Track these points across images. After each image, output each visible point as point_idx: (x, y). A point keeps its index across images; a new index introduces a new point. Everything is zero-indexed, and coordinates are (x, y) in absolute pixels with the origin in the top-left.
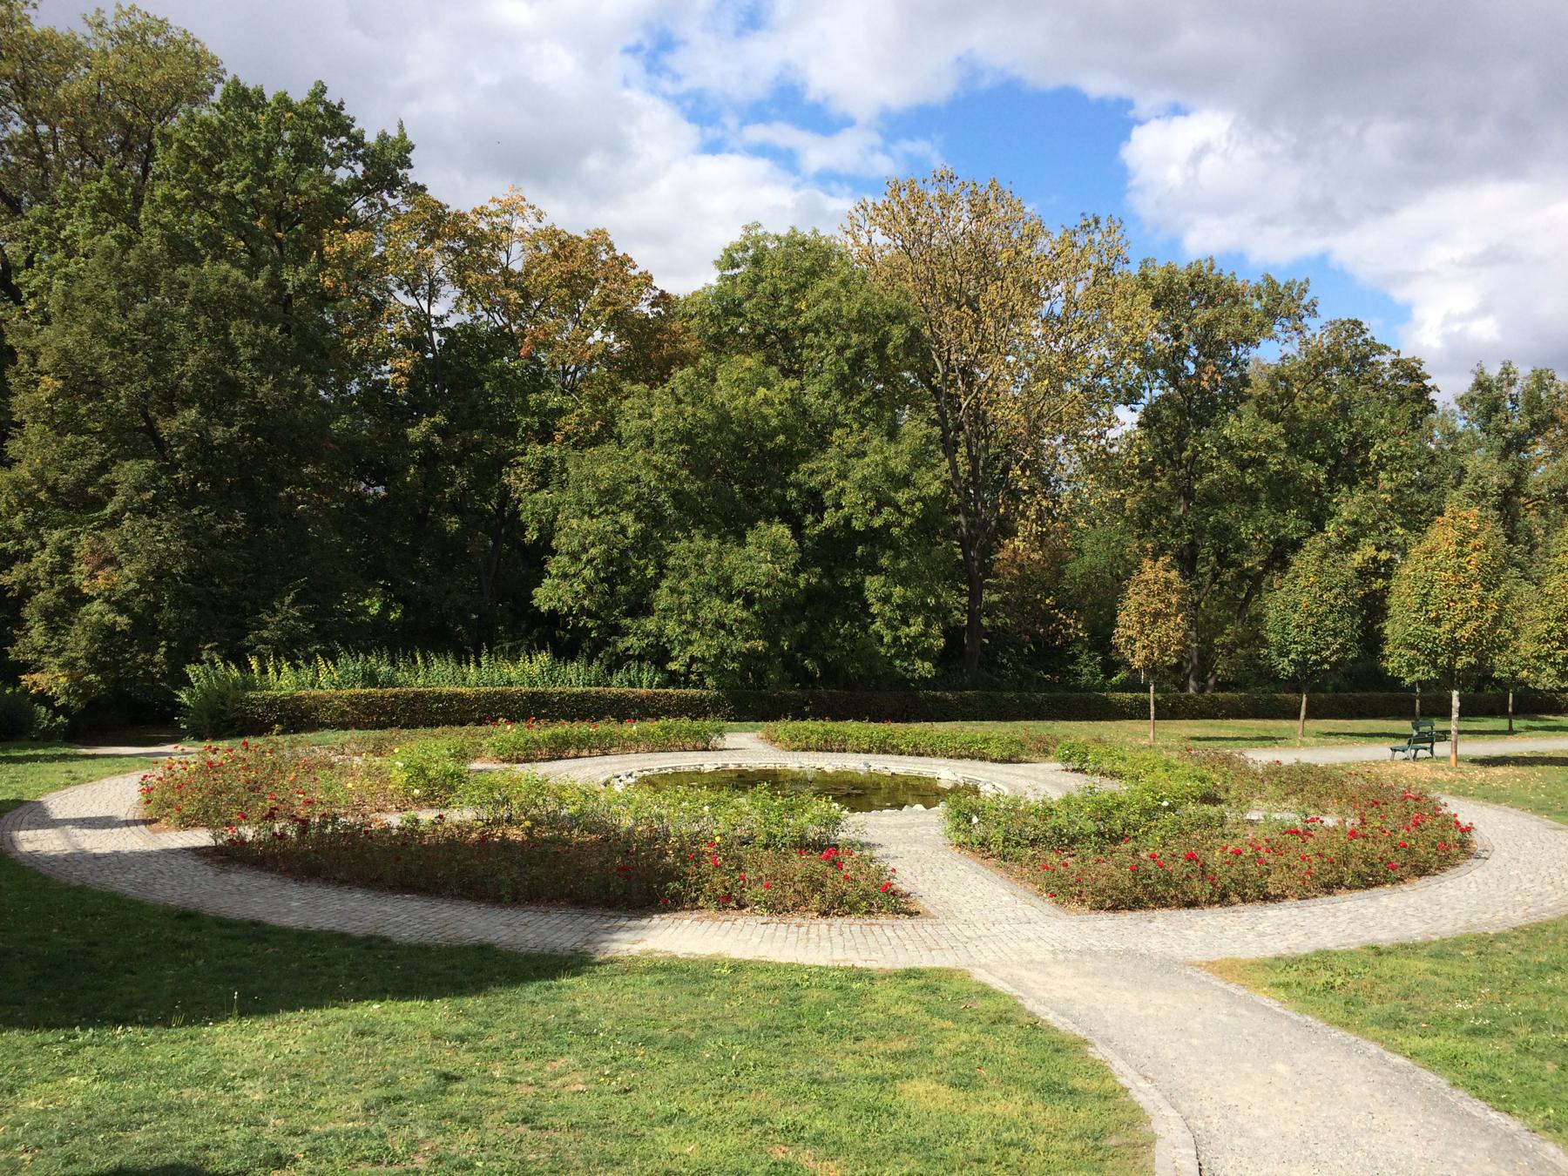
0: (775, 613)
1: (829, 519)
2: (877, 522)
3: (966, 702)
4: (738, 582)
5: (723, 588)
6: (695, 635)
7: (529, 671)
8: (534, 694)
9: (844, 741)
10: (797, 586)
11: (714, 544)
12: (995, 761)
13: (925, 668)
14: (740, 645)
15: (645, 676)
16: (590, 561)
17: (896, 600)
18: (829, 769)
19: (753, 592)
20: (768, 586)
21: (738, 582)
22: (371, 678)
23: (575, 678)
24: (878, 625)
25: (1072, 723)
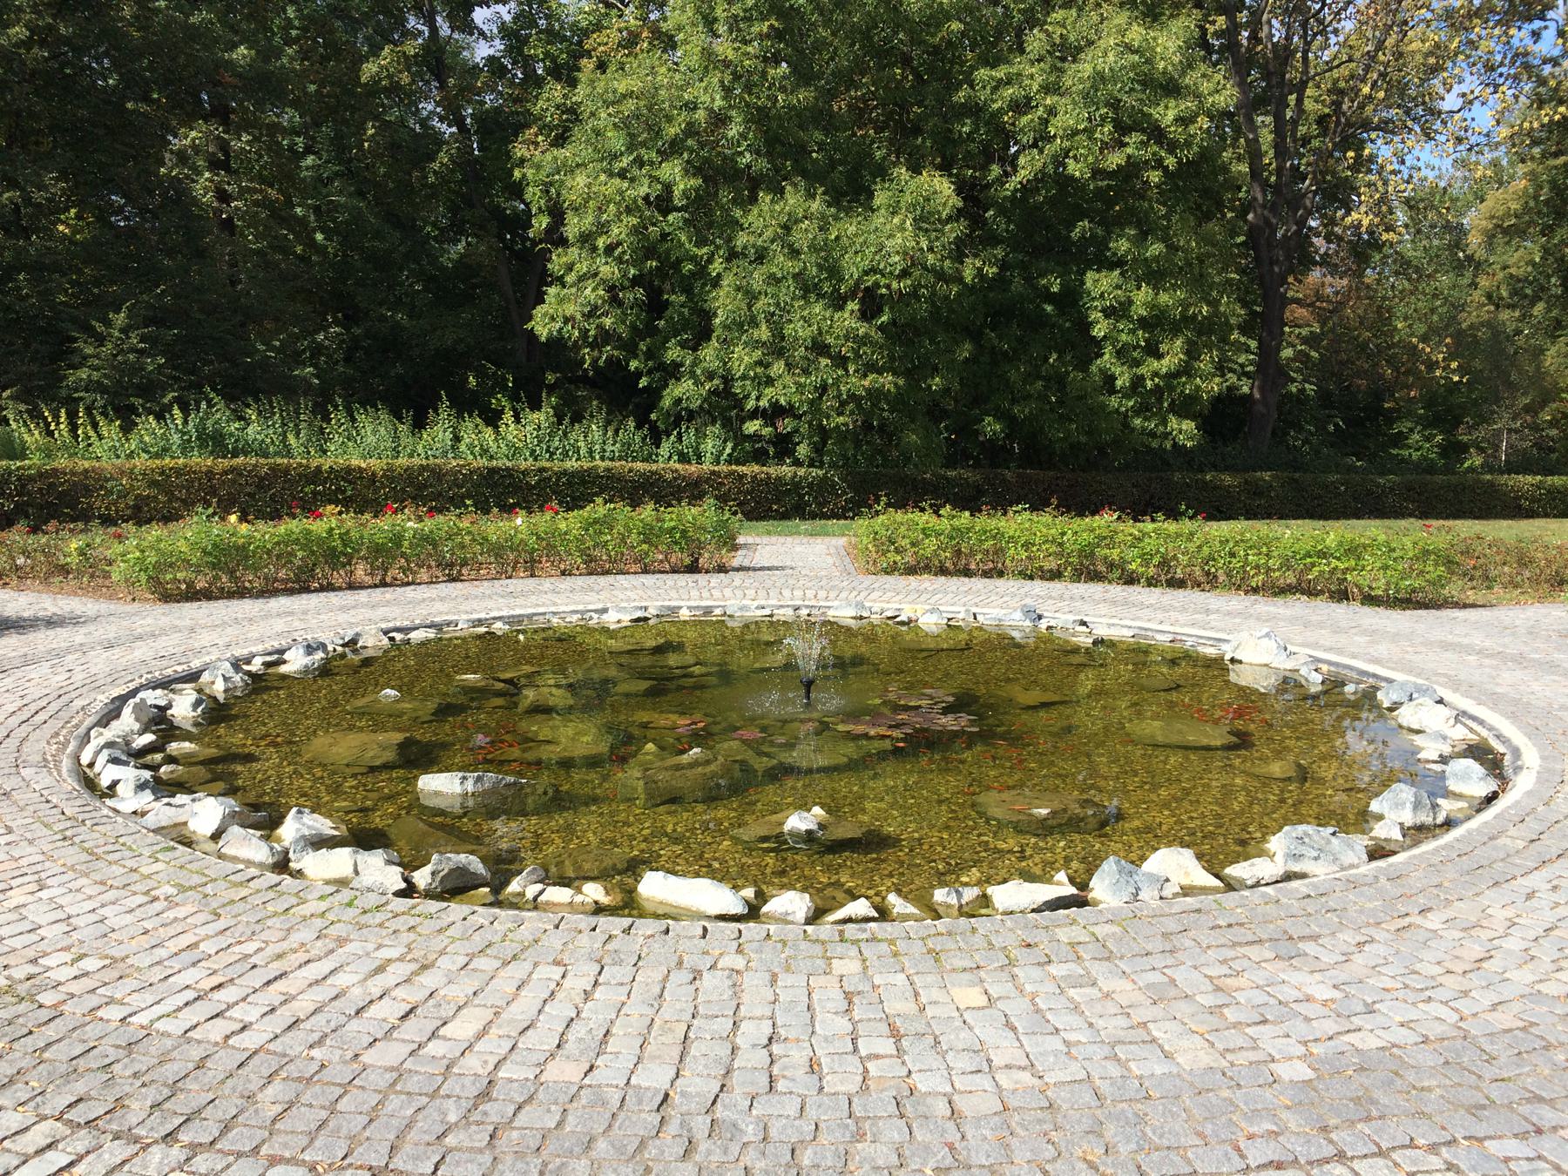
0: (910, 323)
1: (1028, 166)
2: (1115, 160)
3: (1256, 491)
4: (852, 268)
5: (828, 284)
6: (778, 368)
7: (519, 438)
8: (493, 471)
9: (999, 551)
10: (960, 280)
11: (816, 205)
12: (1370, 600)
13: (1184, 430)
14: (857, 383)
15: (709, 446)
16: (609, 250)
17: (1139, 310)
18: (930, 622)
19: (877, 285)
20: (905, 274)
21: (852, 268)
22: (215, 442)
23: (595, 445)
24: (1107, 359)
25: (1492, 522)
